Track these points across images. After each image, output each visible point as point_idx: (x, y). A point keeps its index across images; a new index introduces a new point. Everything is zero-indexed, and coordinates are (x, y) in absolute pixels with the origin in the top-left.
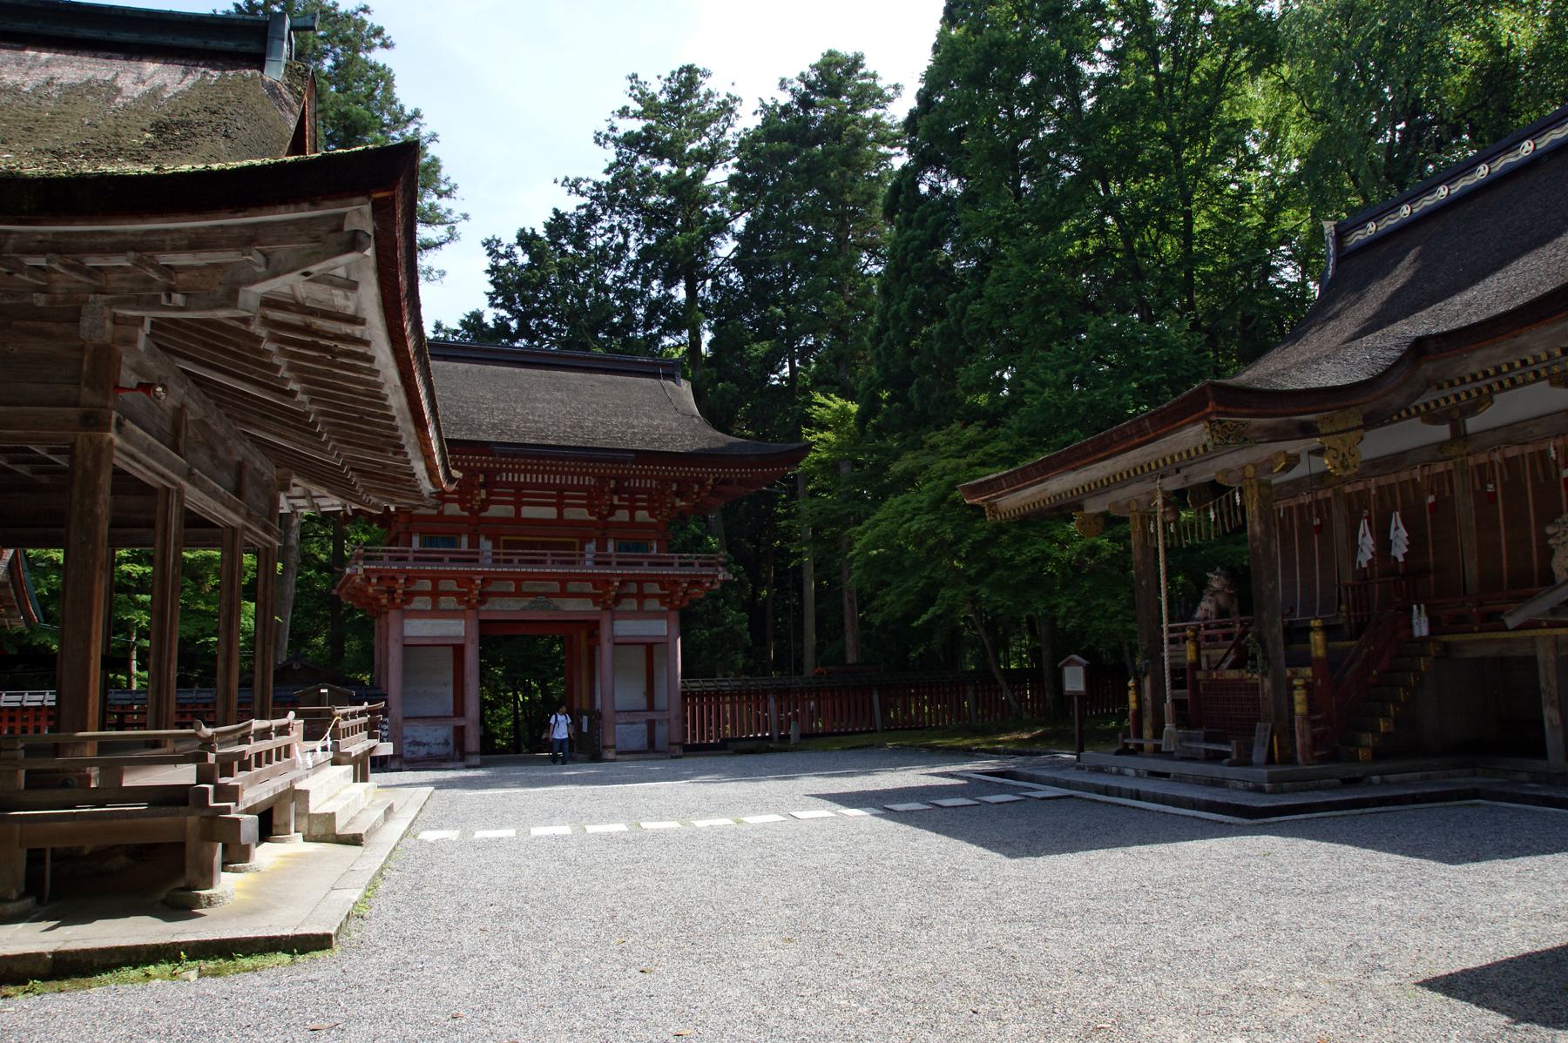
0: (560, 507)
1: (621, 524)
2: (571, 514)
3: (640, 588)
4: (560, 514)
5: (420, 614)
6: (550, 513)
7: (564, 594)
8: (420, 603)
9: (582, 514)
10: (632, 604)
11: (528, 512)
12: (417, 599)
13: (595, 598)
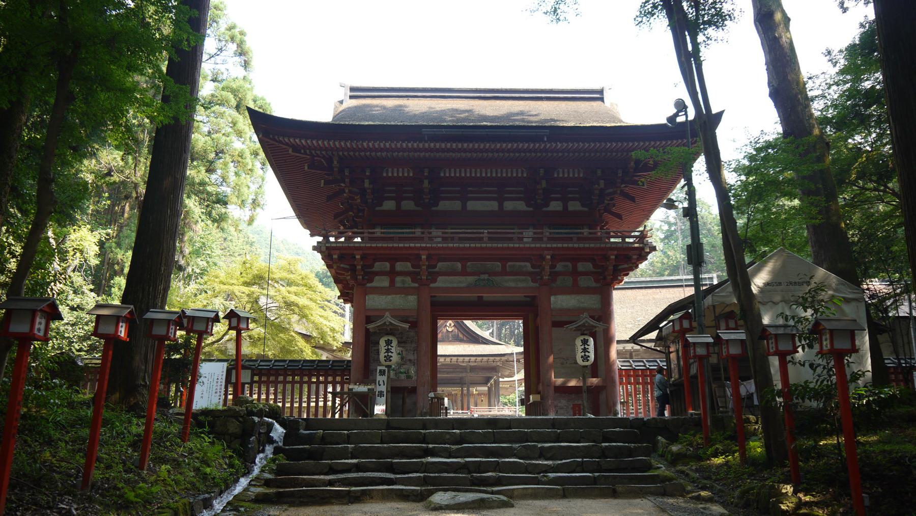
2: (509, 206)
4: (501, 206)
5: (381, 291)
6: (493, 206)
8: (382, 282)
9: (521, 206)
11: (472, 205)
12: (440, 278)
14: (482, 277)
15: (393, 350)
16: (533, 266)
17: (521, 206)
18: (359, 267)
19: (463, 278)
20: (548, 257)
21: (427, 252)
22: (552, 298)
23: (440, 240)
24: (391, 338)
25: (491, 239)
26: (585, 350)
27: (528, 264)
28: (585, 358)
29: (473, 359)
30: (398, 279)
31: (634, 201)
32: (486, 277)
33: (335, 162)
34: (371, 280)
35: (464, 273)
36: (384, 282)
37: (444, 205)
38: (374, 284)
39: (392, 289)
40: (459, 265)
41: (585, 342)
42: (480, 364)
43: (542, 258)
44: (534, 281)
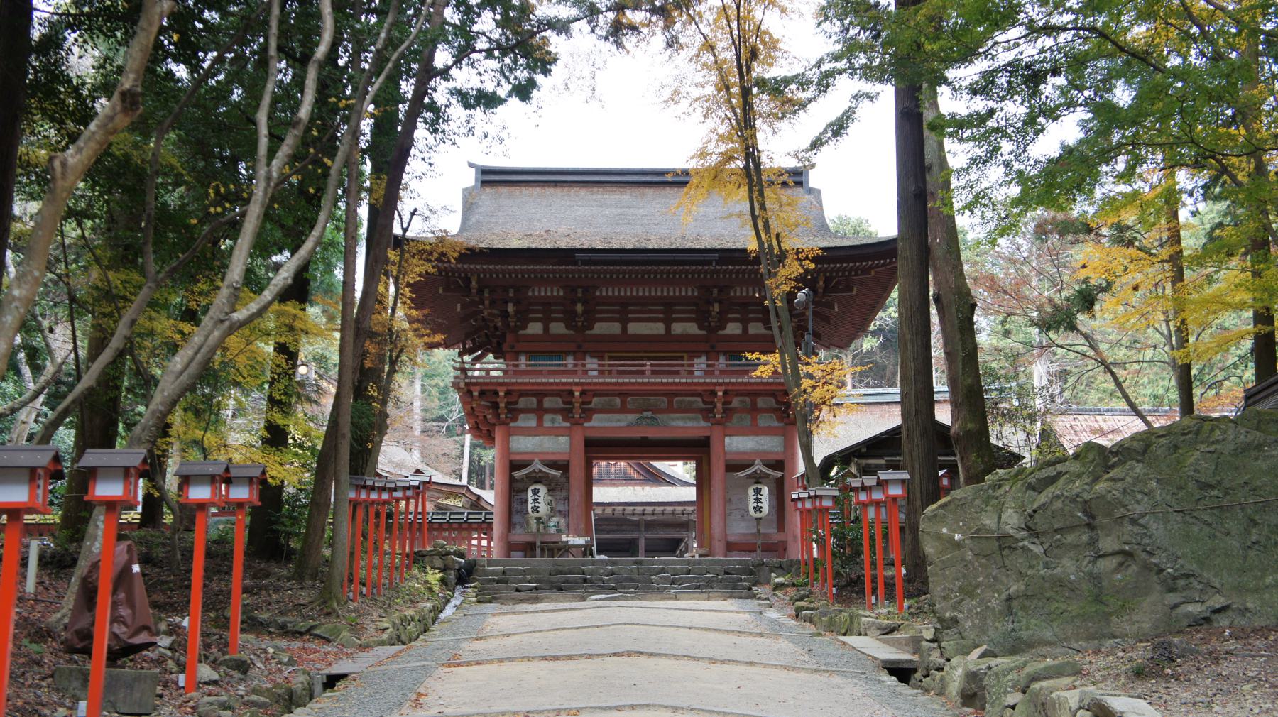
0: (668, 322)
1: (533, 338)
2: (678, 328)
3: (540, 402)
4: (668, 329)
6: (658, 328)
7: (670, 409)
9: (692, 329)
10: (529, 421)
11: (633, 328)
13: (707, 413)
14: (645, 414)
15: (540, 500)
16: (704, 402)
17: (692, 329)
18: (502, 405)
19: (621, 416)
20: (720, 394)
21: (580, 388)
22: (727, 440)
23: (595, 373)
24: (538, 486)
25: (653, 372)
26: (757, 500)
27: (699, 399)
28: (758, 510)
29: (649, 509)
30: (547, 418)
31: (829, 323)
32: (649, 414)
33: (473, 283)
34: (515, 419)
35: (623, 410)
36: (531, 422)
37: (600, 328)
38: (520, 423)
39: (538, 431)
40: (618, 400)
41: (758, 491)
42: (661, 517)
43: (714, 393)
44: (706, 419)
